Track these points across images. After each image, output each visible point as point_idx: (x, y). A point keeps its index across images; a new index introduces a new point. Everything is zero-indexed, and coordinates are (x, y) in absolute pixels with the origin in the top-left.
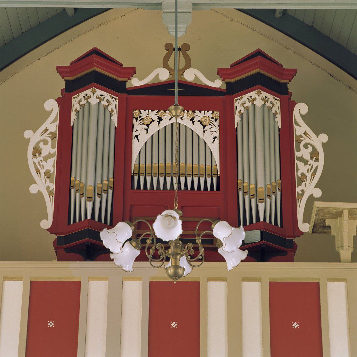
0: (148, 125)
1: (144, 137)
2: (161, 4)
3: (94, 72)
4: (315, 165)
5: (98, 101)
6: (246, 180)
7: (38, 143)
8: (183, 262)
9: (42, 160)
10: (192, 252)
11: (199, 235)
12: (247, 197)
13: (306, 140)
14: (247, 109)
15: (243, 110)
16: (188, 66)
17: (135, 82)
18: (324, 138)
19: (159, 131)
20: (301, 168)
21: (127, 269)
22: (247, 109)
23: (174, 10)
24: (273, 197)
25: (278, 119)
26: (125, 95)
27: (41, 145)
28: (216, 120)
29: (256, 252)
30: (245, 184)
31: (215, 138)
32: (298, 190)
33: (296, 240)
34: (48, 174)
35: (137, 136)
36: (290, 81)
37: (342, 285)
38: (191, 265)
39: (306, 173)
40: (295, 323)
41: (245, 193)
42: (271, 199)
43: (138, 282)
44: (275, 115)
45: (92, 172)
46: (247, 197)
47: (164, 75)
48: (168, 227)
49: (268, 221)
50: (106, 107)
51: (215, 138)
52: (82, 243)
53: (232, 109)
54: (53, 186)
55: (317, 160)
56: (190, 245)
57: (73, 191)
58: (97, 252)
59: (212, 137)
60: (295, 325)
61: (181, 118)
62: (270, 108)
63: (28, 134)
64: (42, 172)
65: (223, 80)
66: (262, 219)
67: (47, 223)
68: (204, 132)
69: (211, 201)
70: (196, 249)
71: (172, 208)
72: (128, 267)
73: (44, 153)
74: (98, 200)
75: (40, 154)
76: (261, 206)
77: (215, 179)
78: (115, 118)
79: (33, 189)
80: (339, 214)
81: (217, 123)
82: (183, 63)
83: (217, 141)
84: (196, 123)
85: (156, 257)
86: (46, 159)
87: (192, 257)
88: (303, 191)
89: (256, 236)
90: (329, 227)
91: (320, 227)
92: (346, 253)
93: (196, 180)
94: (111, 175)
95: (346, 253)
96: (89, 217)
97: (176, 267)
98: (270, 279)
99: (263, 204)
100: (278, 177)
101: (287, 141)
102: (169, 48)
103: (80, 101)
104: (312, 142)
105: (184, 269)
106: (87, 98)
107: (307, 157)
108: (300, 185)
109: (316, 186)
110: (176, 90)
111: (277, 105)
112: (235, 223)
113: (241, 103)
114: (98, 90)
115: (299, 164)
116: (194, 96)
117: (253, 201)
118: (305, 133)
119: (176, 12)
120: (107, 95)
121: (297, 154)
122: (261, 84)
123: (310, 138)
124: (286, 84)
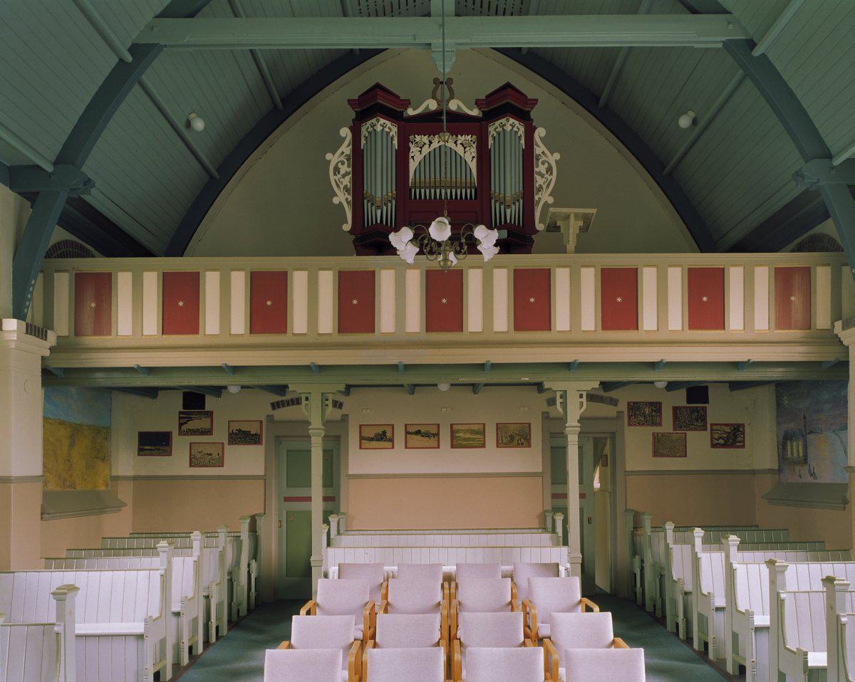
0: (421, 148)
1: (419, 158)
2: (430, 44)
3: (373, 104)
4: (549, 178)
5: (382, 128)
6: (497, 191)
7: (337, 163)
8: (451, 256)
10: (458, 249)
11: (463, 234)
13: (544, 158)
14: (499, 133)
16: (452, 97)
17: (411, 112)
18: (557, 156)
20: (539, 181)
21: (409, 262)
22: (499, 133)
23: (442, 50)
25: (523, 141)
26: (403, 123)
27: (340, 165)
28: (474, 143)
29: (505, 246)
31: (473, 157)
32: (536, 198)
33: (534, 237)
35: (413, 157)
38: (457, 258)
39: (542, 184)
44: (520, 137)
45: (381, 186)
46: (497, 204)
47: (432, 105)
48: (440, 231)
49: (513, 223)
50: (388, 133)
51: (473, 157)
52: (373, 241)
53: (487, 133)
54: (350, 198)
55: (551, 174)
56: (456, 243)
57: (365, 201)
58: (386, 249)
59: (471, 156)
62: (516, 132)
63: (329, 156)
64: (342, 187)
65: (480, 109)
66: (508, 222)
67: (347, 227)
68: (465, 152)
69: (469, 211)
70: (461, 245)
71: (443, 216)
72: (410, 260)
73: (342, 172)
74: (385, 208)
75: (339, 173)
76: (508, 211)
77: (473, 191)
78: (395, 142)
79: (336, 201)
80: (567, 217)
81: (475, 145)
82: (447, 94)
83: (475, 160)
84: (459, 145)
85: (431, 253)
86: (344, 176)
87: (457, 253)
88: (540, 199)
89: (505, 234)
90: (559, 227)
91: (553, 228)
92: (571, 245)
94: (394, 187)
95: (571, 245)
96: (379, 222)
97: (446, 260)
99: (510, 210)
100: (521, 189)
101: (528, 158)
102: (437, 82)
103: (368, 128)
104: (547, 159)
105: (452, 262)
106: (373, 126)
107: (544, 171)
108: (537, 194)
109: (550, 195)
110: (444, 118)
111: (522, 129)
112: (490, 227)
113: (493, 129)
114: (381, 119)
115: (537, 178)
116: (458, 123)
118: (543, 153)
119: (444, 51)
120: (389, 124)
121: (536, 169)
122: (510, 112)
124: (529, 112)
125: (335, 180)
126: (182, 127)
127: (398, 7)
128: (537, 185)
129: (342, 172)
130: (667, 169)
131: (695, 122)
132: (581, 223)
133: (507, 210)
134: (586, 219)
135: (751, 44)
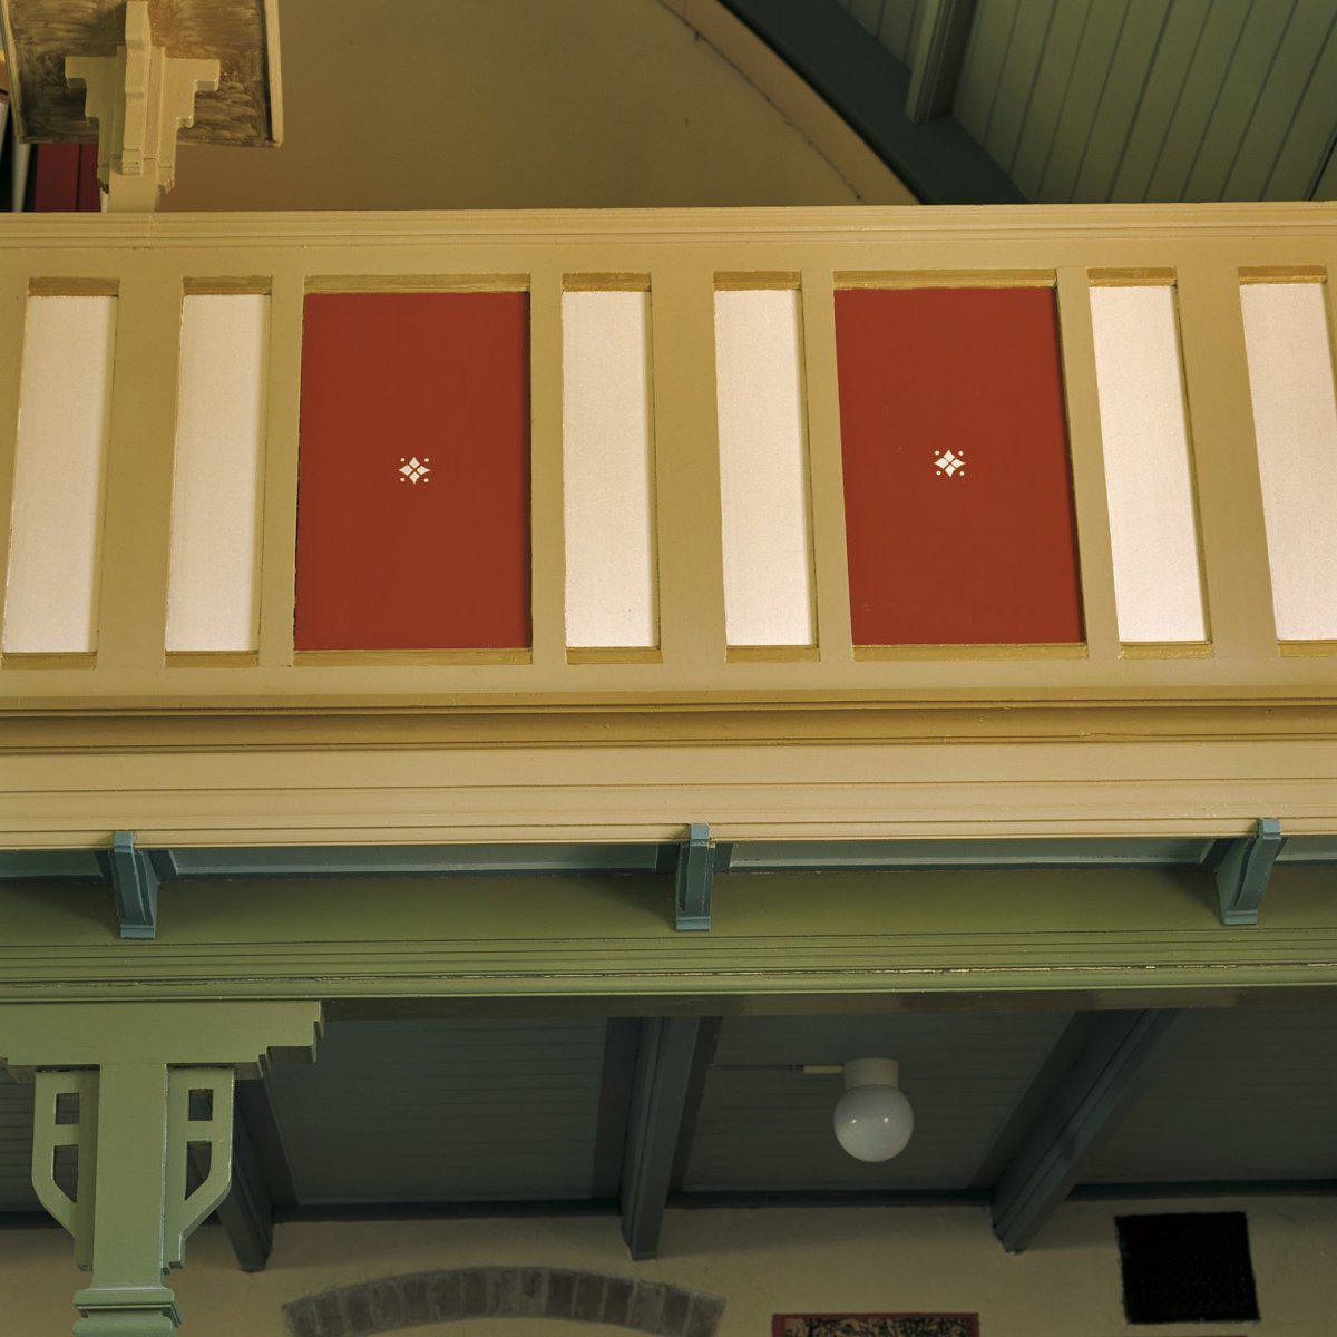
37: (1158, 298)
98: (839, 276)
132: (209, 72)
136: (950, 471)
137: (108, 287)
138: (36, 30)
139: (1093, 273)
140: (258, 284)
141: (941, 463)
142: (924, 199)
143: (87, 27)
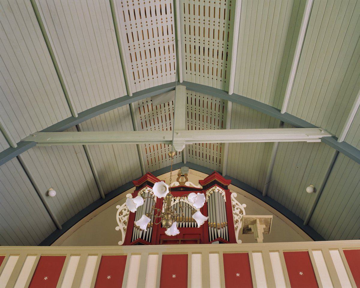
9: (123, 216)
12: (212, 229)
14: (211, 194)
15: (210, 195)
16: (187, 180)
18: (244, 205)
19: (174, 205)
20: (236, 218)
24: (224, 228)
25: (225, 198)
27: (123, 211)
30: (212, 223)
32: (235, 226)
34: (125, 223)
36: (229, 185)
37: (260, 254)
40: (238, 274)
41: (211, 227)
42: (223, 229)
43: (156, 255)
44: (223, 196)
46: (212, 229)
49: (222, 237)
54: (126, 227)
60: (238, 275)
61: (184, 200)
64: (122, 221)
65: (201, 185)
73: (124, 214)
76: (219, 231)
79: (117, 229)
80: (254, 222)
82: (185, 180)
86: (124, 216)
88: (237, 226)
91: (246, 230)
93: (190, 224)
98: (223, 252)
100: (226, 221)
101: (229, 207)
107: (238, 213)
111: (224, 193)
115: (234, 216)
117: (215, 230)
118: (237, 204)
121: (233, 212)
123: (238, 205)
125: (119, 218)
126: (43, 194)
127: (151, 110)
128: (235, 220)
129: (124, 214)
130: (305, 223)
131: (315, 190)
132: (264, 226)
133: (218, 230)
134: (266, 222)
135: (335, 138)
136: (238, 276)
137: (140, 254)
138: (246, 222)
139: (312, 250)
140: (278, 251)
141: (237, 275)
142: (315, 241)
143: (252, 222)
